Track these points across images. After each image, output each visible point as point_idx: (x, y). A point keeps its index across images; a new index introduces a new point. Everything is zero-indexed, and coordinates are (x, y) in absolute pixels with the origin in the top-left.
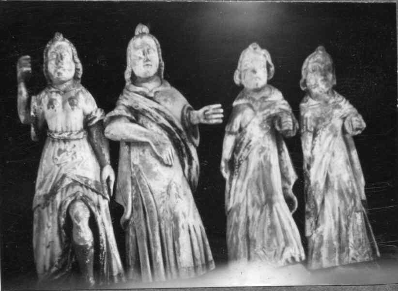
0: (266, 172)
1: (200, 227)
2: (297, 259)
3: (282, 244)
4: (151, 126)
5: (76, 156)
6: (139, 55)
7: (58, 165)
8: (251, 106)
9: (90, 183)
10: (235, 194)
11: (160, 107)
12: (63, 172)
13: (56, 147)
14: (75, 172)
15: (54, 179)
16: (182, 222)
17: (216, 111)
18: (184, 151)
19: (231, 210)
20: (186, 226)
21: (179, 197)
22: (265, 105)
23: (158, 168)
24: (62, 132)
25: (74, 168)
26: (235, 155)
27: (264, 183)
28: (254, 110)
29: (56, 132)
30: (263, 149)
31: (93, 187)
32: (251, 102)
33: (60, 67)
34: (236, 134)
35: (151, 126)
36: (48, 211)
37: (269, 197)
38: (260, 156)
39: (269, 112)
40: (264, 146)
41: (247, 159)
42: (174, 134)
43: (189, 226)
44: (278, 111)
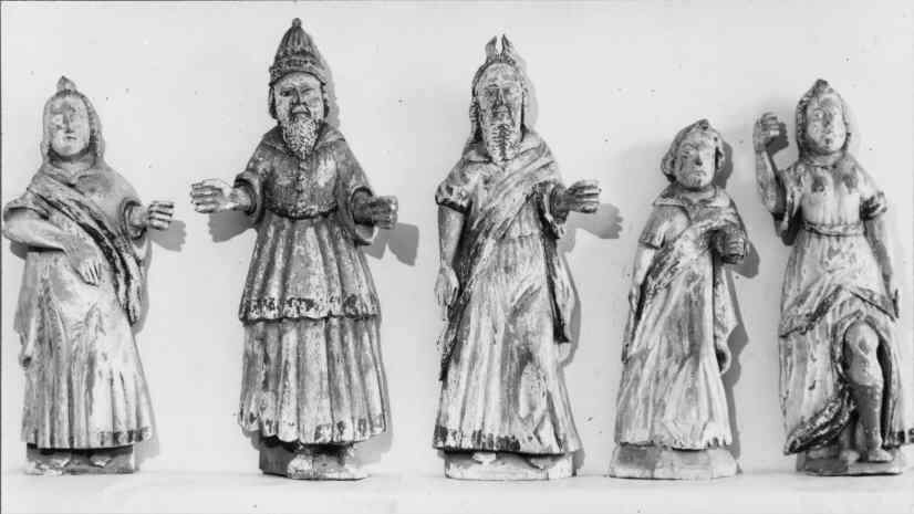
0: (695, 312)
1: (135, 377)
2: (721, 443)
3: (705, 417)
4: (70, 226)
5: (856, 261)
6: (58, 123)
7: (830, 272)
8: (683, 209)
9: (876, 298)
10: (641, 337)
11: (85, 200)
12: (837, 282)
13: (824, 245)
14: (854, 283)
15: (822, 293)
16: (100, 365)
17: (162, 210)
18: (118, 263)
19: (631, 357)
20: (106, 376)
21: (102, 330)
22: (705, 211)
23: (75, 286)
24: (832, 226)
25: (855, 277)
26: (650, 278)
27: (691, 327)
28: (689, 219)
29: (823, 225)
30: (693, 277)
31: (879, 304)
32: (686, 205)
33: (829, 132)
34: (656, 248)
35: (70, 226)
36: (813, 337)
37: (696, 348)
38: (688, 285)
39: (710, 224)
40: (696, 271)
41: (668, 287)
42: (103, 240)
43: (111, 373)
44: (723, 223)
